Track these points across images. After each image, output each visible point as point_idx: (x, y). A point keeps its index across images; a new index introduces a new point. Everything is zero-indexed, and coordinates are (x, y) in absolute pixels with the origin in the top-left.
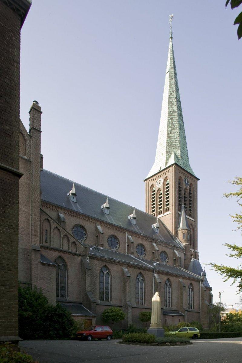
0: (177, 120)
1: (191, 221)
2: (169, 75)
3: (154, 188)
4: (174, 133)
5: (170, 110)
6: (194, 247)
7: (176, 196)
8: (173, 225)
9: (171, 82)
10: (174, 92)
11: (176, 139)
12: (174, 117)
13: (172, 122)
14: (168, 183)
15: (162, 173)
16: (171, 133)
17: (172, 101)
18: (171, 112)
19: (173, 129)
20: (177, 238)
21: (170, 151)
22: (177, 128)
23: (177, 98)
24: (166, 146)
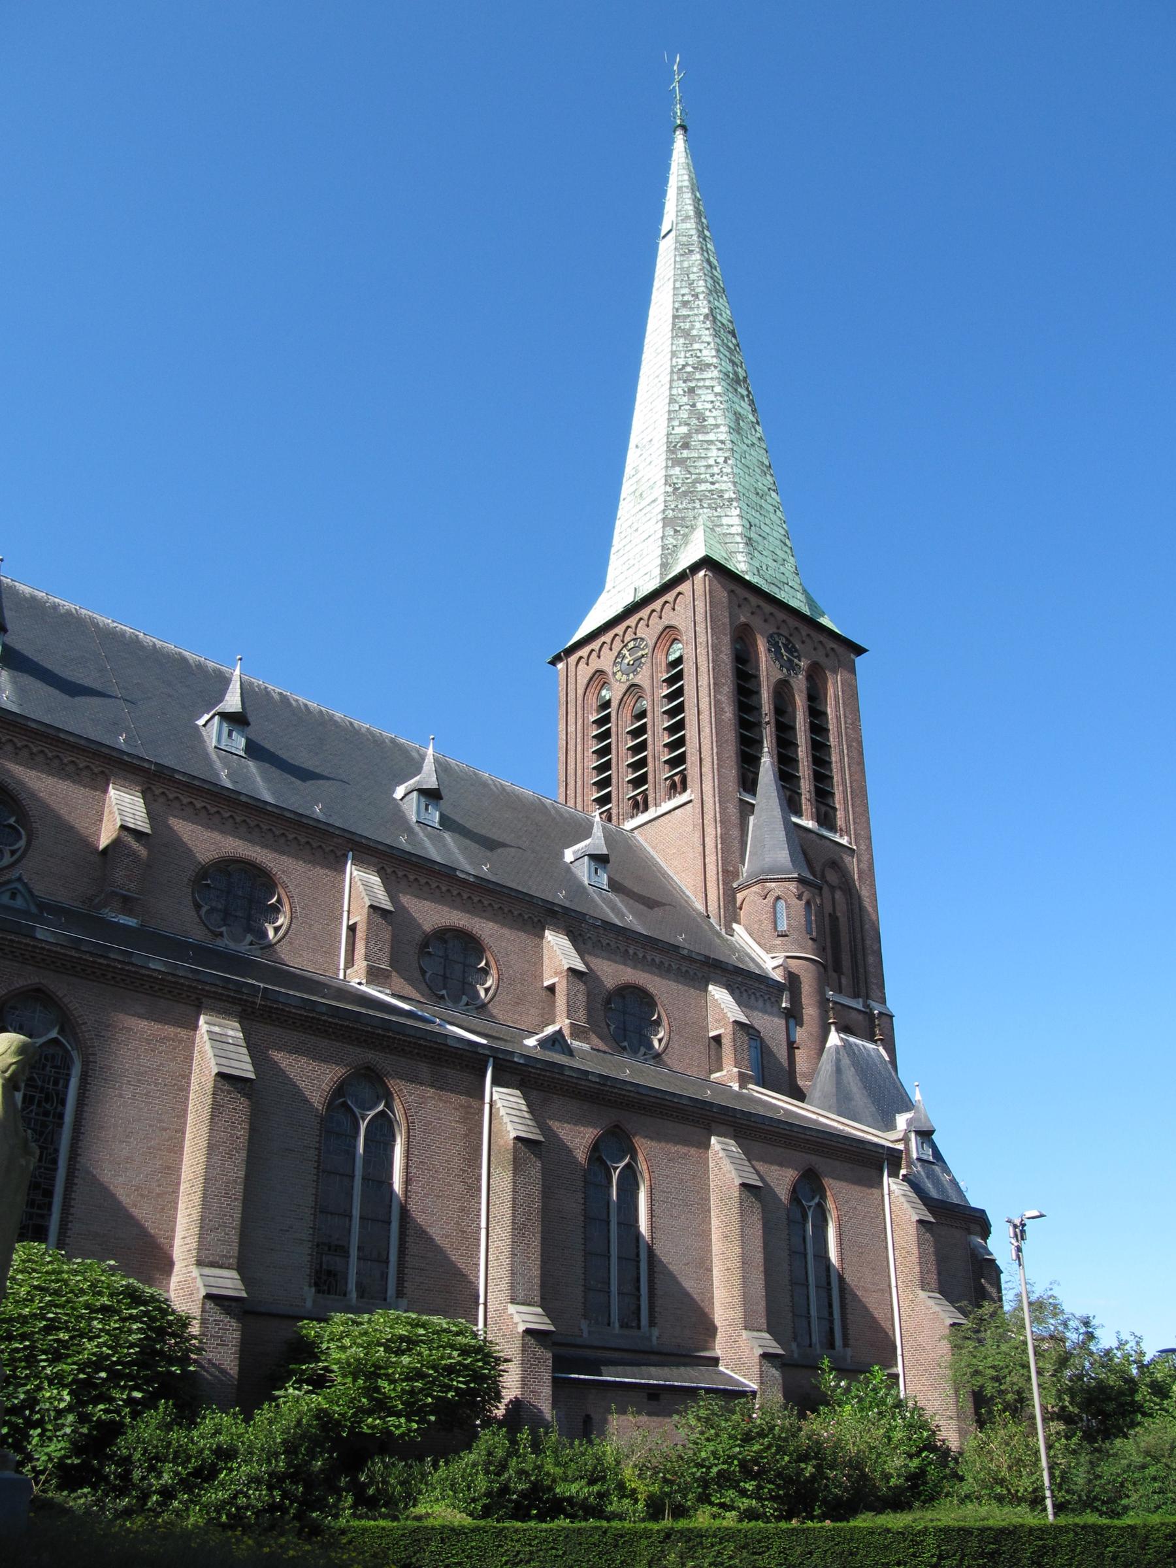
0: (717, 394)
1: (832, 845)
2: (673, 241)
3: (604, 692)
4: (705, 446)
5: (682, 362)
6: (862, 985)
7: (719, 711)
8: (711, 859)
9: (686, 264)
10: (701, 297)
11: (716, 470)
12: (701, 384)
13: (694, 405)
14: (677, 655)
15: (644, 613)
16: (686, 446)
17: (693, 327)
18: (684, 366)
19: (697, 432)
20: (735, 926)
21: (683, 518)
22: (717, 426)
23: (715, 318)
24: (662, 499)
